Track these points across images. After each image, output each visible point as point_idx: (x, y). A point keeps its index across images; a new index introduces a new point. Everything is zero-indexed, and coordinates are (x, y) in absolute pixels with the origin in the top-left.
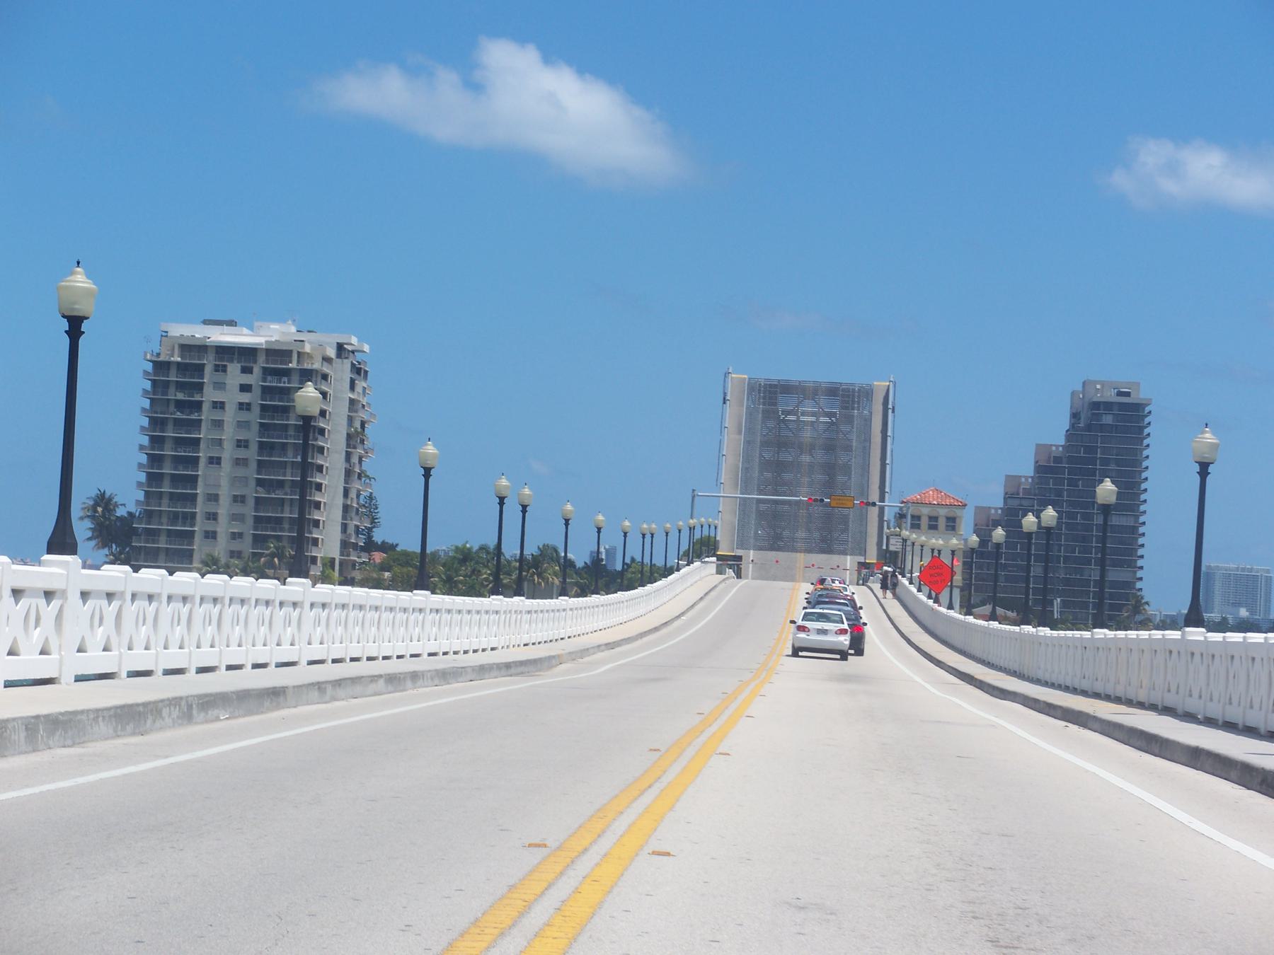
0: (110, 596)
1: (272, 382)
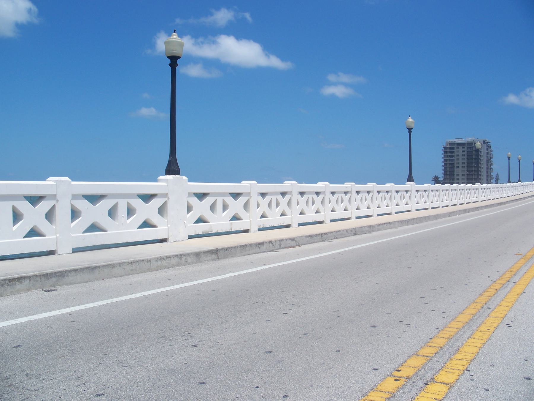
0: (437, 191)
1: (469, 150)
